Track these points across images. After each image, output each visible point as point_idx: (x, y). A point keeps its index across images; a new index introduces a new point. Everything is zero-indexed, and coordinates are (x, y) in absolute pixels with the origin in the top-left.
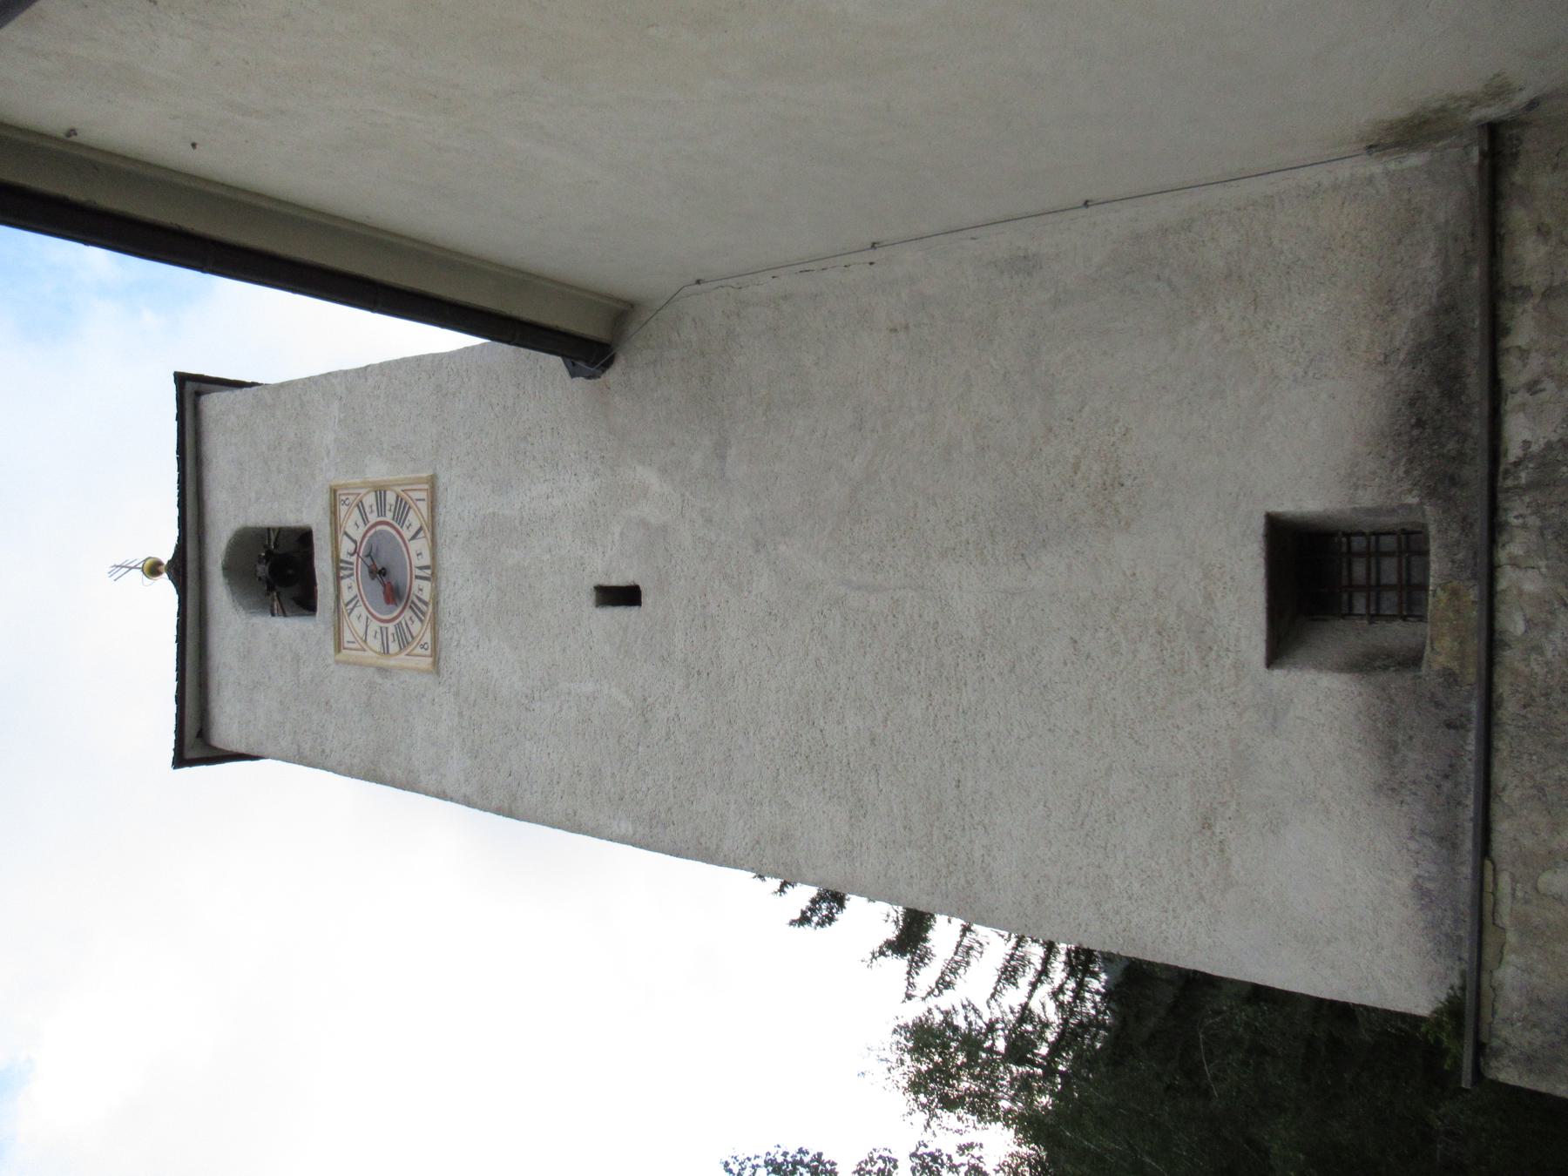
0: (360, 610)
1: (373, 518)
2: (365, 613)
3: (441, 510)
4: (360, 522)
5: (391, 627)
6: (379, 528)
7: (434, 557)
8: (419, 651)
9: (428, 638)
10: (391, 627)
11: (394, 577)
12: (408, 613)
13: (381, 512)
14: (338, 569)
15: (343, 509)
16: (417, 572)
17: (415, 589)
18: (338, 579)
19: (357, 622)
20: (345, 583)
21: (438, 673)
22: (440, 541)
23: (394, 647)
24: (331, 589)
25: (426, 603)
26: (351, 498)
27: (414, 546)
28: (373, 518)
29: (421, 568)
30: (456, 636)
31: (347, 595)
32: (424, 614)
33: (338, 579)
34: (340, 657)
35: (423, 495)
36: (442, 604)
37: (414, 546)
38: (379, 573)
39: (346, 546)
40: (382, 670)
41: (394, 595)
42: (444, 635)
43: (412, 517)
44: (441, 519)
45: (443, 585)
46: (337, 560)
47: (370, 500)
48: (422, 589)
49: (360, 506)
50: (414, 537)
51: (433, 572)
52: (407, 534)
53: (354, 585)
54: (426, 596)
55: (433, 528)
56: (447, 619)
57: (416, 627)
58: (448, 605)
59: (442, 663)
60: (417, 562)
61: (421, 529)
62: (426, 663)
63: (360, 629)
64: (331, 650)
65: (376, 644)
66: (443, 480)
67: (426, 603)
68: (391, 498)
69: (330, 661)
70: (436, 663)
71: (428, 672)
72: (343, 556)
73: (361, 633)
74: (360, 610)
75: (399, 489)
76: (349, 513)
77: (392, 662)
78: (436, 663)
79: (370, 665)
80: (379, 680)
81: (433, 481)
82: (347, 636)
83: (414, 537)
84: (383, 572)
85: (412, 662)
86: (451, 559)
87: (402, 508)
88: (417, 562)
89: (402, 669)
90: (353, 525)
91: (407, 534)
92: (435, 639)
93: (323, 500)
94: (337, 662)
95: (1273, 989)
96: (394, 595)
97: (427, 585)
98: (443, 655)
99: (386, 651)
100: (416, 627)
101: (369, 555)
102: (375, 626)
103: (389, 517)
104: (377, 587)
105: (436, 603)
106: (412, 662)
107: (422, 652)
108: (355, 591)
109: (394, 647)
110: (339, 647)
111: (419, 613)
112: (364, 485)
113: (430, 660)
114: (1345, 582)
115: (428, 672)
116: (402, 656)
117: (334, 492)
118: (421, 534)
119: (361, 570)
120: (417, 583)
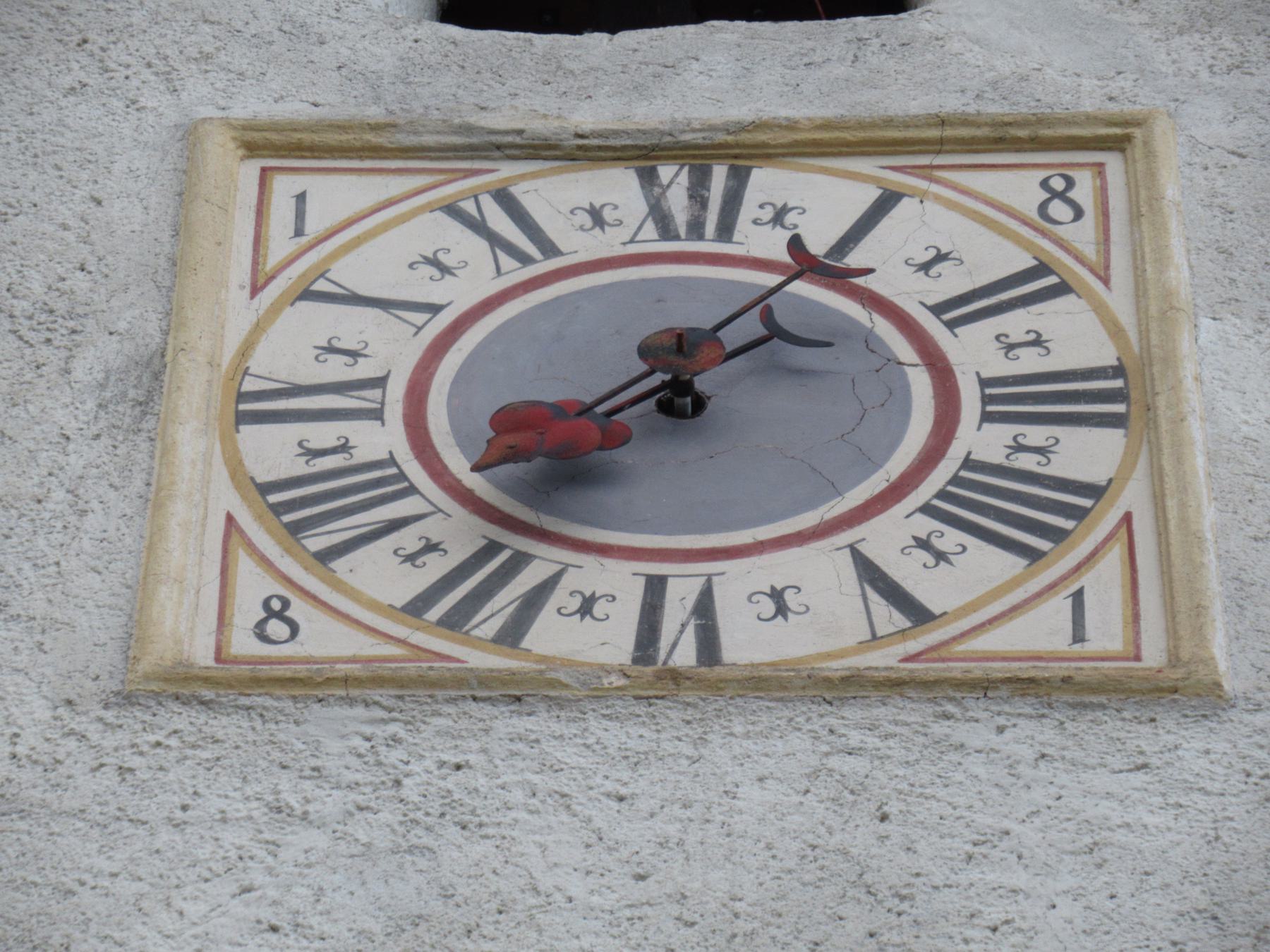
0: (476, 274)
1: (974, 352)
2: (460, 294)
3: (1027, 733)
4: (950, 283)
5: (382, 440)
6: (921, 383)
7: (766, 684)
8: (252, 588)
9: (322, 640)
10: (382, 440)
11: (657, 466)
12: (462, 535)
13: (1003, 399)
14: (697, 154)
15: (1019, 187)
16: (682, 592)
17: (590, 574)
18: (643, 154)
19: (409, 252)
20: (619, 188)
21: (127, 699)
22: (851, 719)
23: (273, 451)
24: (589, 117)
25: (511, 635)
26: (1083, 235)
27: (821, 574)
28: (974, 352)
29: (704, 608)
30: (330, 803)
31: (554, 197)
32: (454, 622)
33: (643, 154)
34: (220, 151)
35: (1105, 634)
36: (506, 722)
37: (821, 574)
38: (677, 381)
39: (822, 203)
40: (146, 385)
41: (553, 458)
42: (336, 732)
43: (983, 565)
44: (976, 728)
45: (616, 733)
46: (726, 155)
47: (1073, 337)
48: (589, 610)
49: (1039, 283)
50: (871, 574)
51: (678, 675)
52: (887, 539)
53: (609, 243)
54: (552, 635)
55: (927, 685)
56: (430, 747)
57: (382, 575)
58: (499, 754)
59: (183, 719)
60: (737, 585)
61: (919, 615)
62: (186, 629)
63: (376, 267)
64: (253, 105)
65: (292, 349)
66: (1192, 747)
67: (511, 635)
68: (1085, 453)
69: (200, 96)
70: (184, 686)
71: (135, 633)
72: (765, 183)
73: (351, 273)
74: (476, 274)
75: (1133, 497)
76: (993, 218)
77: (192, 438)
78: (184, 686)
79: (172, 318)
80: (86, 367)
81: (1181, 690)
82: (336, 194)
83: (871, 574)
84: (679, 401)
85: (189, 552)
86: (760, 773)
87: (1027, 516)
88: (737, 585)
89: (154, 501)
90: (932, 241)
91: (887, 539)
92: (314, 684)
93: (1070, 80)
94: (190, 135)
95: (865, 234)
96: (553, 458)
97: (611, 641)
98: (228, 726)
99: (251, 407)
100: (382, 575)
101: (774, 332)
102: (393, 348)
103: (980, 440)
104: (599, 368)
105: (514, 692)
106: (189, 552)
107: (247, 611)
108: (579, 244)
109: (273, 451)
110: (274, 146)
111: (452, 601)
112: (1155, 307)
113: (203, 655)
114: (466, 628)
115: (135, 633)
116: (227, 499)
117: (1116, 137)
118: (888, 618)
119: (701, 289)
120: (621, 584)
